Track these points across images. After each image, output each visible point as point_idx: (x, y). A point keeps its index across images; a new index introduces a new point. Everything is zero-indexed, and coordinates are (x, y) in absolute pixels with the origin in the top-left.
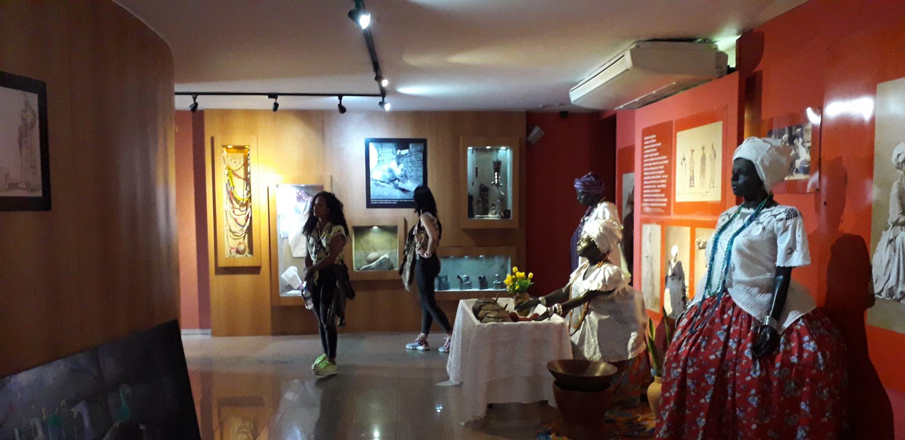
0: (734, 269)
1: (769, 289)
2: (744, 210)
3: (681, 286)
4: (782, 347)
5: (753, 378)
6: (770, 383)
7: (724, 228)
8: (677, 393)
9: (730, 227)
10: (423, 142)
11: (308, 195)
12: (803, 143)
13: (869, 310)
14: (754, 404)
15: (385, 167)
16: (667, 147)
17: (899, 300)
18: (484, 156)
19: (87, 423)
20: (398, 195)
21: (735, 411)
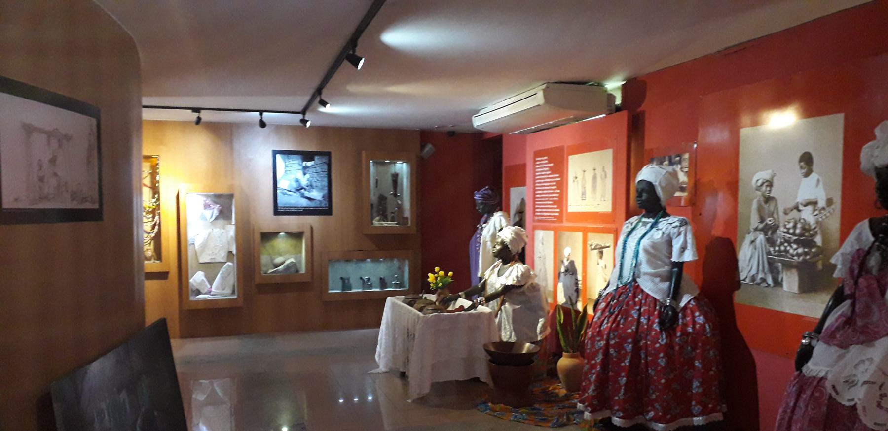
0: (640, 264)
1: (669, 279)
2: (644, 220)
3: (573, 282)
4: (681, 321)
5: (661, 345)
6: (673, 348)
7: (630, 233)
8: (603, 360)
9: (634, 233)
10: (328, 154)
11: (216, 203)
12: (681, 168)
13: (736, 292)
14: (662, 364)
15: (292, 177)
16: (559, 167)
17: (759, 284)
18: (382, 169)
19: (128, 407)
20: (304, 203)
21: (647, 371)
